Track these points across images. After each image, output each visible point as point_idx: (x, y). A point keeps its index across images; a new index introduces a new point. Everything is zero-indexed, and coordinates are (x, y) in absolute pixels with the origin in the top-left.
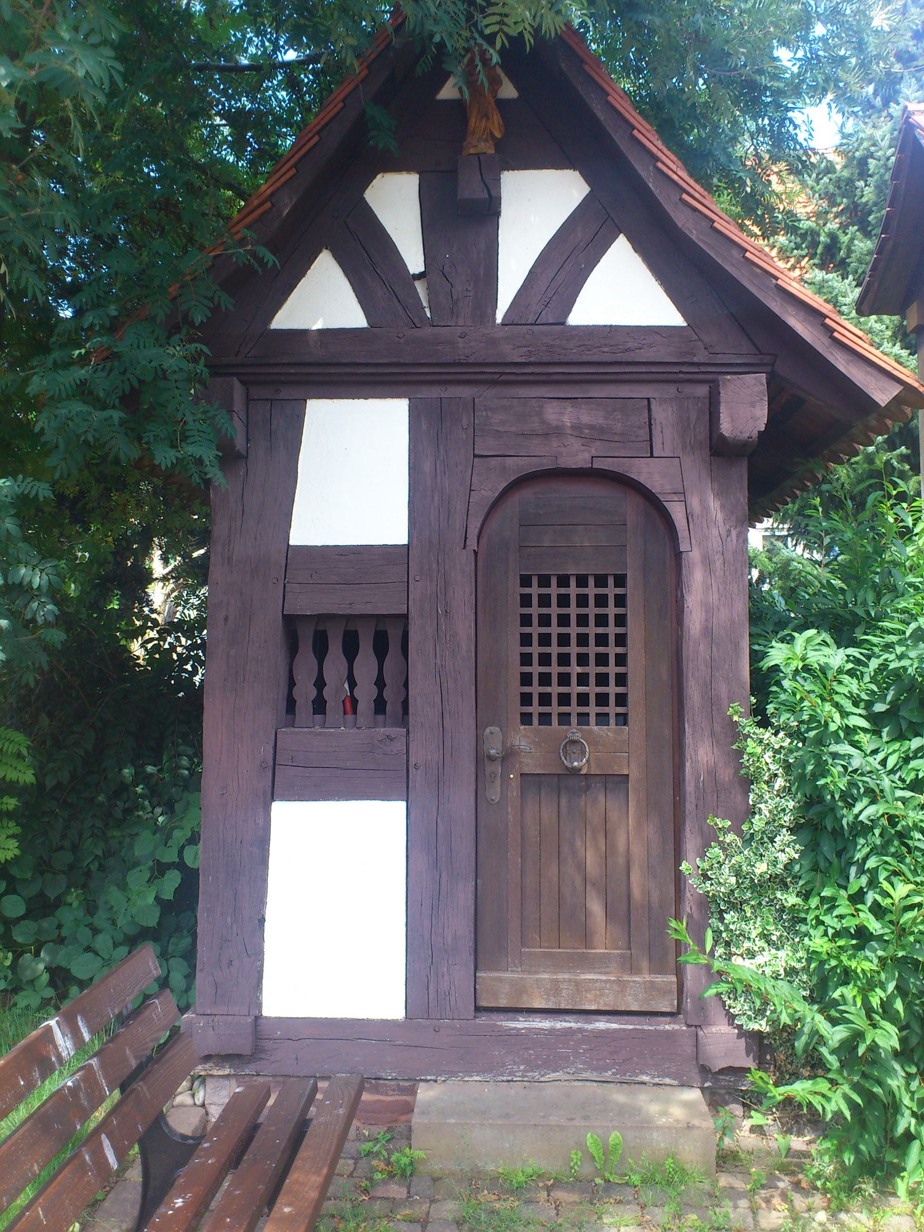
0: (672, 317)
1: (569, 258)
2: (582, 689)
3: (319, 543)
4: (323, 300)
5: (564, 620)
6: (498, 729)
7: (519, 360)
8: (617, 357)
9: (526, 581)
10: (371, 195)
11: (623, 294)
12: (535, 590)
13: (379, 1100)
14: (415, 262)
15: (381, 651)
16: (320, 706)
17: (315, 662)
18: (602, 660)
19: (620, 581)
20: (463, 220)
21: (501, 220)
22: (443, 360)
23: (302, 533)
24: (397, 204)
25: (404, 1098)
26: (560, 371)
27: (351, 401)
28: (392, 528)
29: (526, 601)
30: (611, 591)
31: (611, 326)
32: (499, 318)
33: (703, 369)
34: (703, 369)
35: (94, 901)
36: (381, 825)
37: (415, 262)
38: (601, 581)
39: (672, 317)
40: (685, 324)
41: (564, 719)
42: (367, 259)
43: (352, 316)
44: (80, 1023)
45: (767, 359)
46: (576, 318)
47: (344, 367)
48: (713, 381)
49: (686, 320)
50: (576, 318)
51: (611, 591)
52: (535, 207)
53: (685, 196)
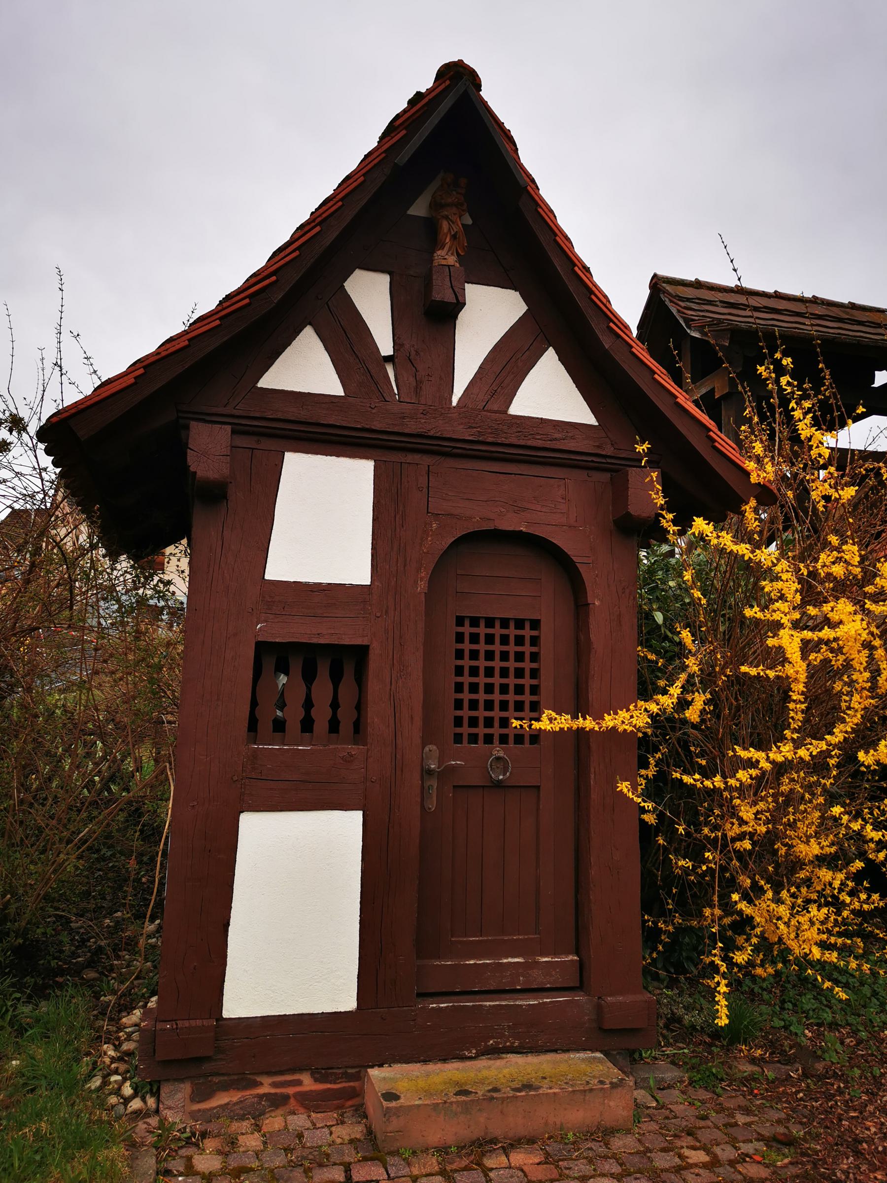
1: (508, 363)
4: (306, 369)
6: (435, 747)
7: (471, 438)
9: (460, 621)
12: (467, 629)
13: (329, 1089)
14: (386, 347)
16: (307, 725)
17: (331, 686)
19: (536, 624)
20: (430, 318)
21: (457, 322)
22: (406, 431)
23: (271, 574)
24: (371, 297)
25: (352, 1084)
26: (552, 455)
27: (334, 458)
28: (357, 570)
29: (460, 638)
30: (527, 632)
31: (542, 419)
32: (454, 403)
33: (609, 461)
34: (609, 461)
37: (386, 347)
38: (520, 624)
40: (597, 424)
41: (489, 739)
42: (346, 340)
44: (505, 961)
47: (320, 429)
48: (617, 471)
49: (598, 421)
50: (518, 408)
51: (527, 632)
53: (611, 325)
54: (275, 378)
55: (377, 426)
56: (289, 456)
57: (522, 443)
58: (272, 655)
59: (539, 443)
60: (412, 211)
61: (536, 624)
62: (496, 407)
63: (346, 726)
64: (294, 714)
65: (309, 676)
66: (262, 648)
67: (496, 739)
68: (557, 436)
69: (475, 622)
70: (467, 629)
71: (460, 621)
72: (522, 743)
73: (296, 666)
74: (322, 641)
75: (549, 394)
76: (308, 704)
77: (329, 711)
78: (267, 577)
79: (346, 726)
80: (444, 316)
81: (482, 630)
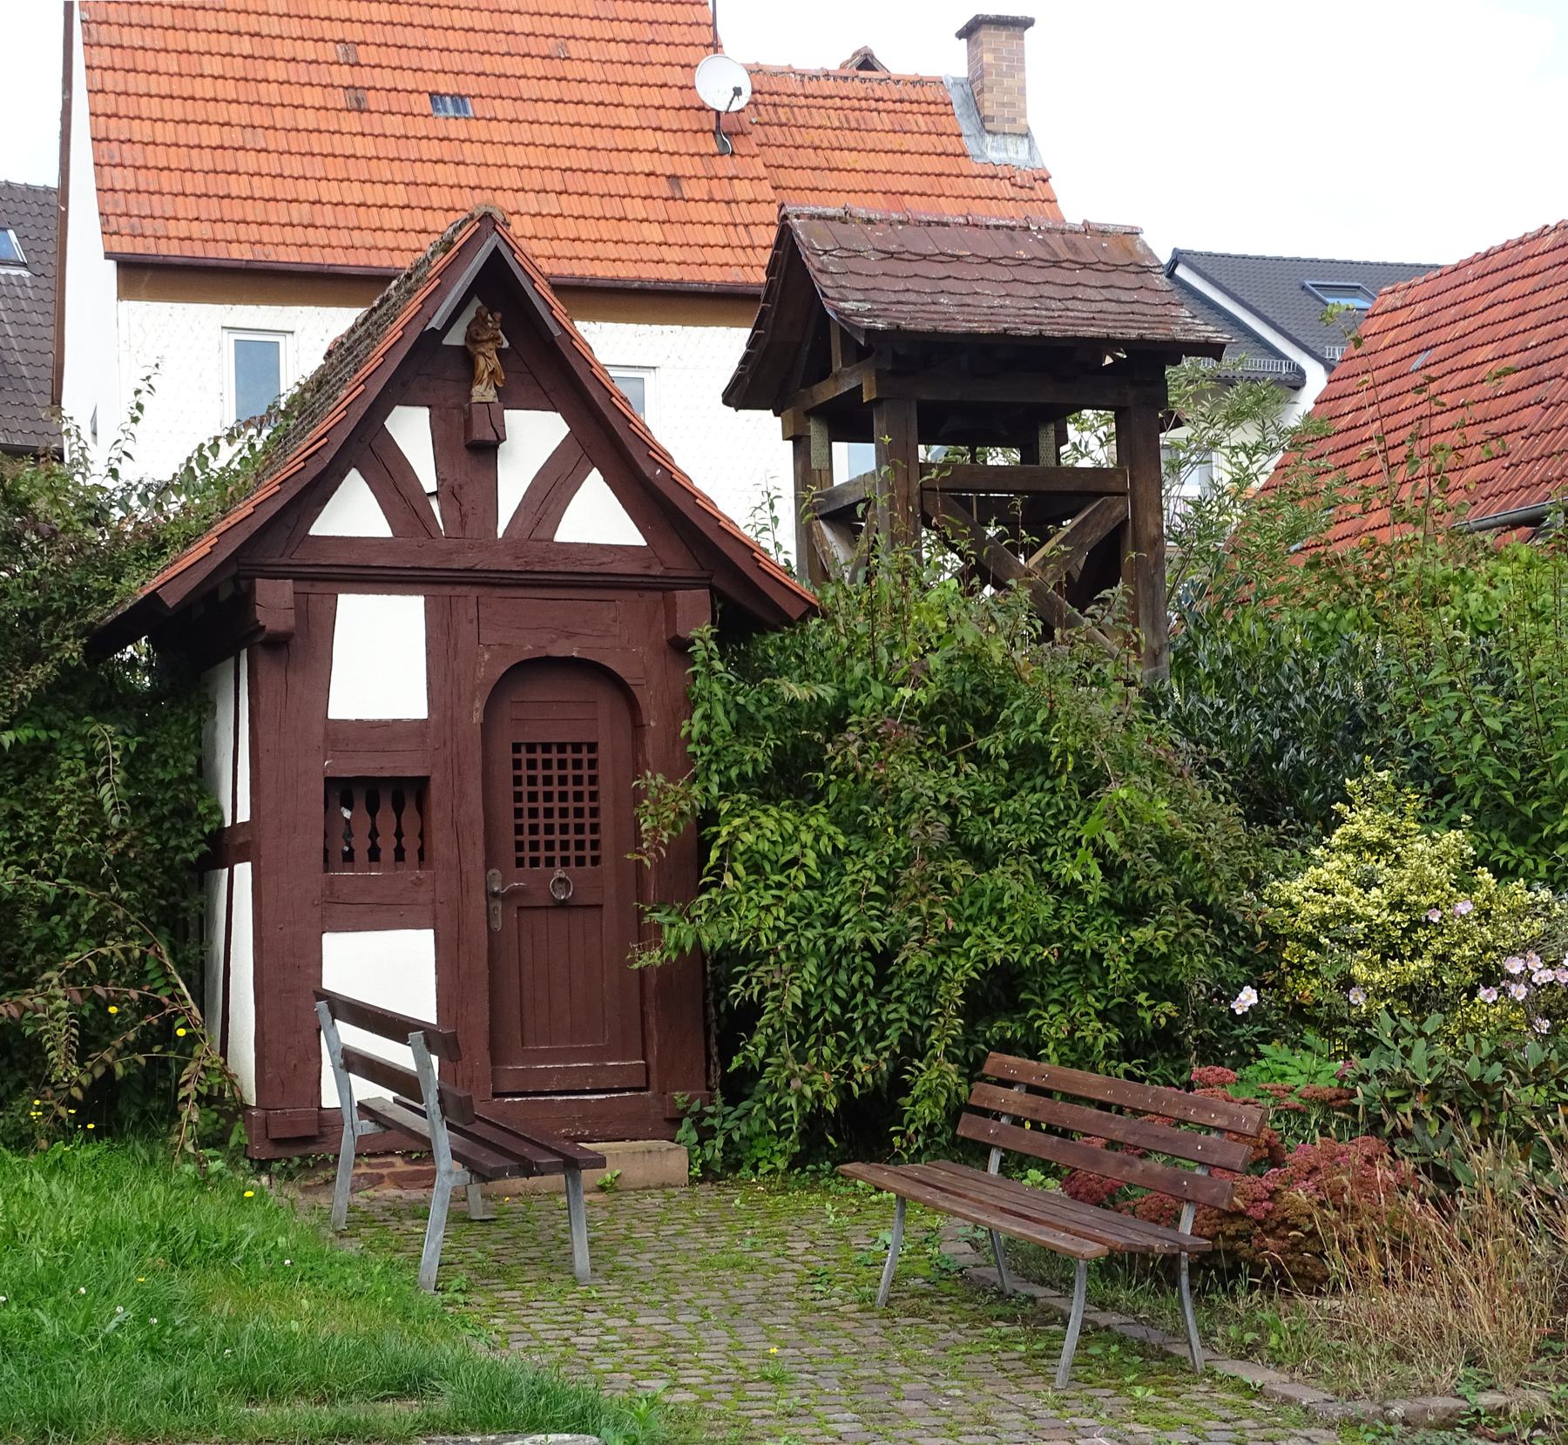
0: (635, 538)
1: (553, 489)
3: (352, 716)
4: (353, 513)
5: (548, 781)
8: (592, 574)
9: (516, 748)
10: (389, 424)
11: (597, 518)
12: (524, 756)
14: (429, 483)
16: (374, 854)
18: (578, 796)
19: (593, 747)
20: (472, 451)
24: (412, 432)
32: (500, 535)
35: (1013, 105)
37: (429, 483)
38: (577, 747)
39: (635, 538)
45: (706, 574)
46: (561, 536)
47: (370, 571)
50: (561, 536)
51: (585, 755)
57: (569, 569)
58: (340, 790)
59: (587, 569)
61: (593, 747)
64: (361, 845)
65: (373, 809)
67: (557, 862)
70: (524, 756)
73: (360, 803)
76: (374, 834)
81: (539, 756)
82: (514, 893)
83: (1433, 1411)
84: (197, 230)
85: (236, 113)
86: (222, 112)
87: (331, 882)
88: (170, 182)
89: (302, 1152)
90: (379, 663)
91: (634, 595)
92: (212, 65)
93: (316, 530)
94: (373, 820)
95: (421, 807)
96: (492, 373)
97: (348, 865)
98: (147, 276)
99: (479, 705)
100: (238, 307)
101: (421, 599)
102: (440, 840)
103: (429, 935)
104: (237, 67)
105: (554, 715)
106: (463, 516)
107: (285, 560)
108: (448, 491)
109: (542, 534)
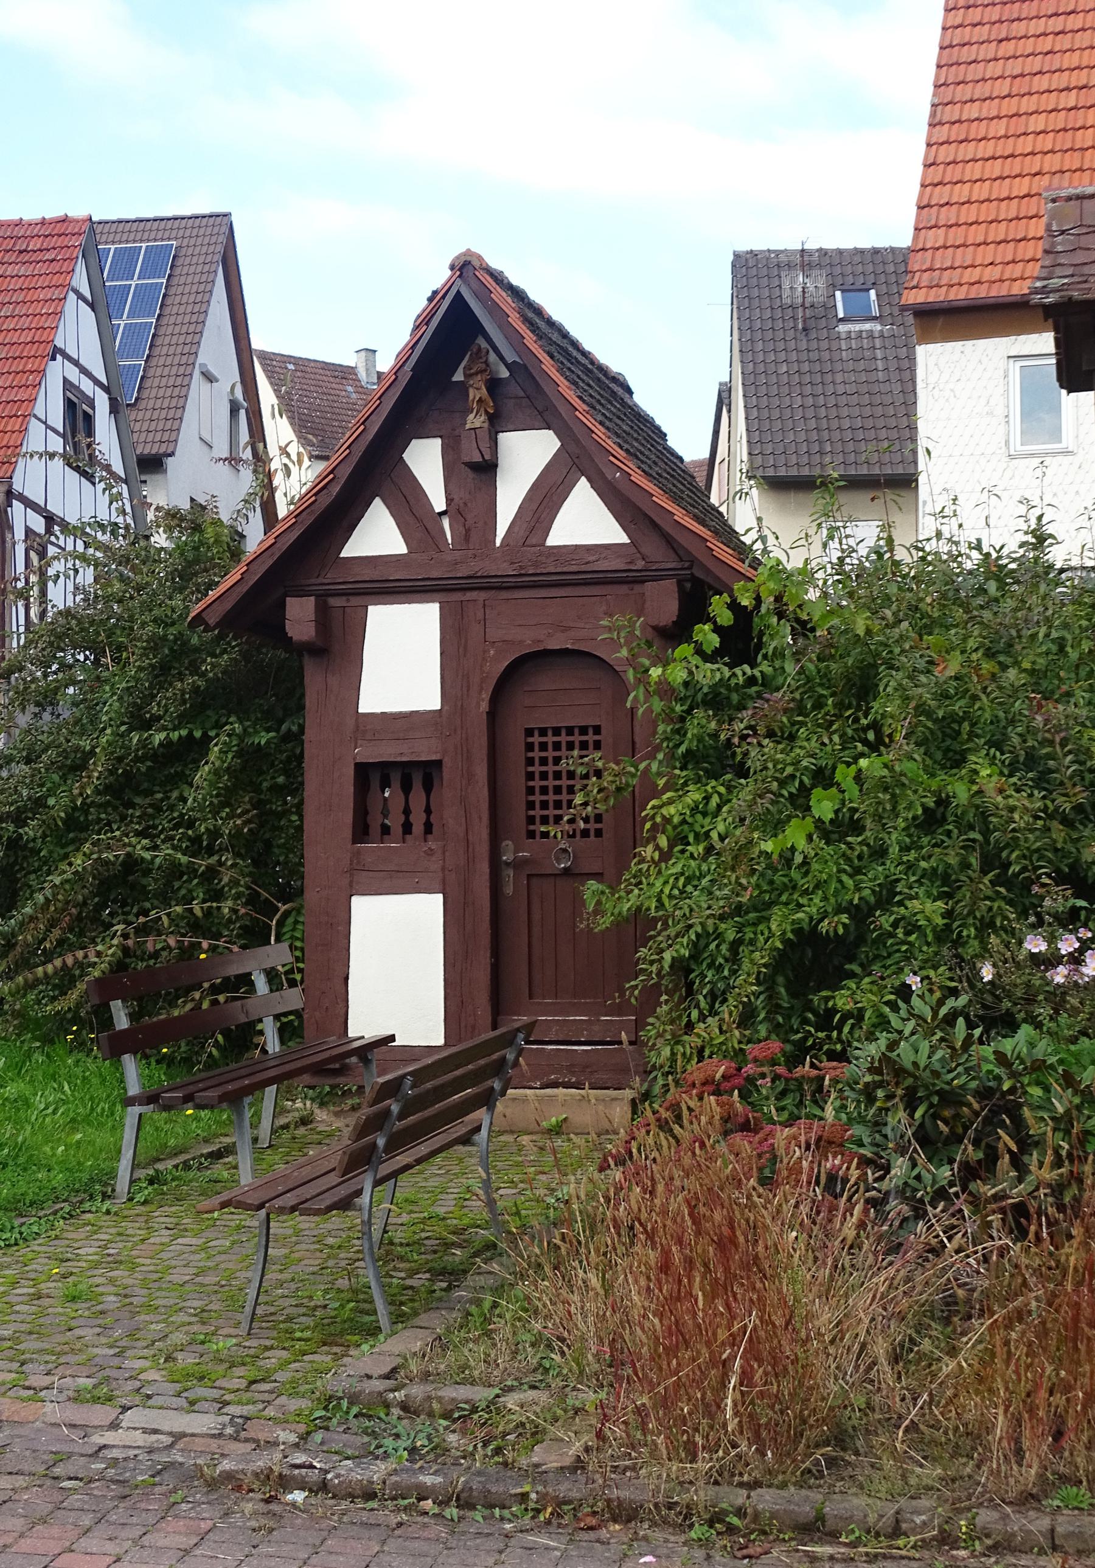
0: (622, 538)
1: (546, 498)
2: (545, 812)
3: (378, 710)
4: (378, 535)
11: (585, 522)
12: (536, 739)
14: (439, 503)
15: (428, 787)
16: (407, 828)
19: (597, 730)
20: (476, 472)
23: (366, 705)
31: (876, 251)
32: (498, 544)
36: (426, 912)
37: (439, 503)
43: (398, 547)
46: (553, 540)
47: (392, 584)
50: (553, 540)
52: (526, 454)
54: (352, 549)
55: (435, 575)
56: (371, 609)
57: (559, 570)
58: (367, 775)
60: (454, 379)
61: (597, 730)
62: (534, 541)
63: (418, 828)
64: (395, 821)
65: (407, 788)
66: (363, 770)
68: (591, 558)
69: (543, 732)
70: (536, 739)
71: (529, 732)
72: (534, 837)
73: (396, 782)
74: (404, 759)
75: (585, 522)
76: (407, 812)
77: (424, 815)
78: (362, 710)
79: (418, 828)
80: (487, 469)
81: (550, 739)
82: (525, 861)
83: (440, 1399)
84: (994, 273)
85: (1052, 162)
86: (1034, 164)
87: (359, 852)
88: (977, 234)
89: (332, 1081)
90: (401, 662)
91: (624, 589)
92: (1038, 123)
93: (344, 554)
94: (398, 796)
95: (428, 787)
96: (480, 400)
97: (386, 837)
98: (941, 321)
99: (486, 696)
100: (1023, 337)
101: (437, 606)
102: (449, 815)
103: (439, 897)
104: (1059, 120)
105: (551, 703)
106: (468, 531)
107: (319, 580)
108: (454, 508)
109: (533, 540)
